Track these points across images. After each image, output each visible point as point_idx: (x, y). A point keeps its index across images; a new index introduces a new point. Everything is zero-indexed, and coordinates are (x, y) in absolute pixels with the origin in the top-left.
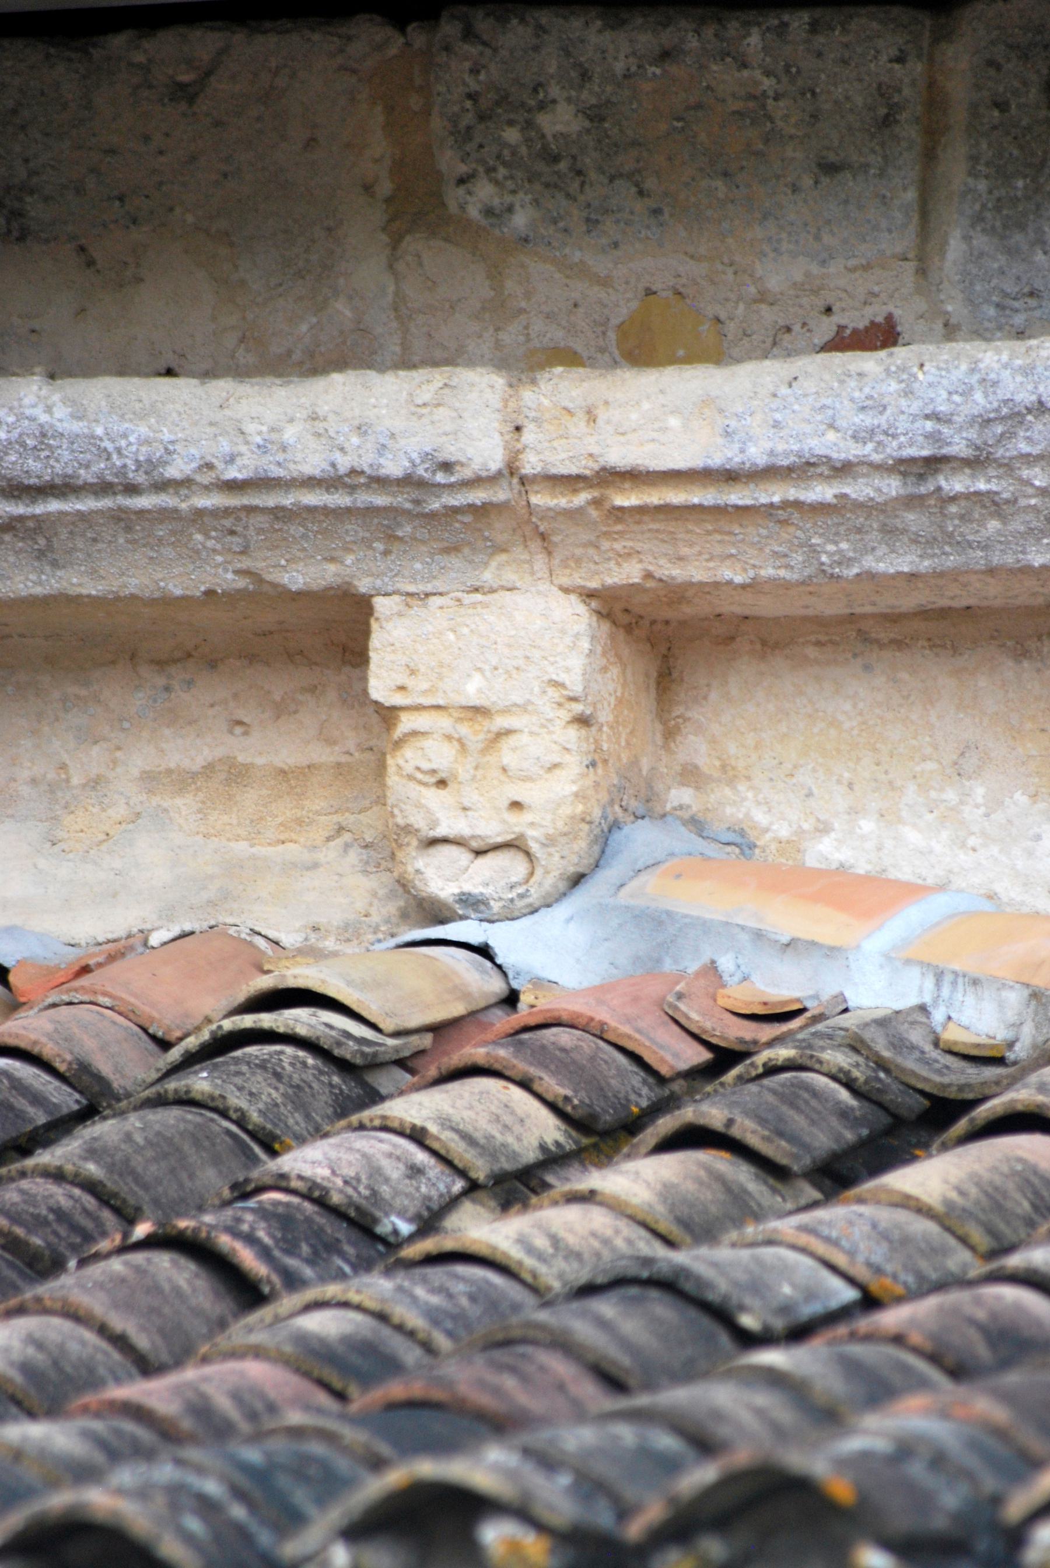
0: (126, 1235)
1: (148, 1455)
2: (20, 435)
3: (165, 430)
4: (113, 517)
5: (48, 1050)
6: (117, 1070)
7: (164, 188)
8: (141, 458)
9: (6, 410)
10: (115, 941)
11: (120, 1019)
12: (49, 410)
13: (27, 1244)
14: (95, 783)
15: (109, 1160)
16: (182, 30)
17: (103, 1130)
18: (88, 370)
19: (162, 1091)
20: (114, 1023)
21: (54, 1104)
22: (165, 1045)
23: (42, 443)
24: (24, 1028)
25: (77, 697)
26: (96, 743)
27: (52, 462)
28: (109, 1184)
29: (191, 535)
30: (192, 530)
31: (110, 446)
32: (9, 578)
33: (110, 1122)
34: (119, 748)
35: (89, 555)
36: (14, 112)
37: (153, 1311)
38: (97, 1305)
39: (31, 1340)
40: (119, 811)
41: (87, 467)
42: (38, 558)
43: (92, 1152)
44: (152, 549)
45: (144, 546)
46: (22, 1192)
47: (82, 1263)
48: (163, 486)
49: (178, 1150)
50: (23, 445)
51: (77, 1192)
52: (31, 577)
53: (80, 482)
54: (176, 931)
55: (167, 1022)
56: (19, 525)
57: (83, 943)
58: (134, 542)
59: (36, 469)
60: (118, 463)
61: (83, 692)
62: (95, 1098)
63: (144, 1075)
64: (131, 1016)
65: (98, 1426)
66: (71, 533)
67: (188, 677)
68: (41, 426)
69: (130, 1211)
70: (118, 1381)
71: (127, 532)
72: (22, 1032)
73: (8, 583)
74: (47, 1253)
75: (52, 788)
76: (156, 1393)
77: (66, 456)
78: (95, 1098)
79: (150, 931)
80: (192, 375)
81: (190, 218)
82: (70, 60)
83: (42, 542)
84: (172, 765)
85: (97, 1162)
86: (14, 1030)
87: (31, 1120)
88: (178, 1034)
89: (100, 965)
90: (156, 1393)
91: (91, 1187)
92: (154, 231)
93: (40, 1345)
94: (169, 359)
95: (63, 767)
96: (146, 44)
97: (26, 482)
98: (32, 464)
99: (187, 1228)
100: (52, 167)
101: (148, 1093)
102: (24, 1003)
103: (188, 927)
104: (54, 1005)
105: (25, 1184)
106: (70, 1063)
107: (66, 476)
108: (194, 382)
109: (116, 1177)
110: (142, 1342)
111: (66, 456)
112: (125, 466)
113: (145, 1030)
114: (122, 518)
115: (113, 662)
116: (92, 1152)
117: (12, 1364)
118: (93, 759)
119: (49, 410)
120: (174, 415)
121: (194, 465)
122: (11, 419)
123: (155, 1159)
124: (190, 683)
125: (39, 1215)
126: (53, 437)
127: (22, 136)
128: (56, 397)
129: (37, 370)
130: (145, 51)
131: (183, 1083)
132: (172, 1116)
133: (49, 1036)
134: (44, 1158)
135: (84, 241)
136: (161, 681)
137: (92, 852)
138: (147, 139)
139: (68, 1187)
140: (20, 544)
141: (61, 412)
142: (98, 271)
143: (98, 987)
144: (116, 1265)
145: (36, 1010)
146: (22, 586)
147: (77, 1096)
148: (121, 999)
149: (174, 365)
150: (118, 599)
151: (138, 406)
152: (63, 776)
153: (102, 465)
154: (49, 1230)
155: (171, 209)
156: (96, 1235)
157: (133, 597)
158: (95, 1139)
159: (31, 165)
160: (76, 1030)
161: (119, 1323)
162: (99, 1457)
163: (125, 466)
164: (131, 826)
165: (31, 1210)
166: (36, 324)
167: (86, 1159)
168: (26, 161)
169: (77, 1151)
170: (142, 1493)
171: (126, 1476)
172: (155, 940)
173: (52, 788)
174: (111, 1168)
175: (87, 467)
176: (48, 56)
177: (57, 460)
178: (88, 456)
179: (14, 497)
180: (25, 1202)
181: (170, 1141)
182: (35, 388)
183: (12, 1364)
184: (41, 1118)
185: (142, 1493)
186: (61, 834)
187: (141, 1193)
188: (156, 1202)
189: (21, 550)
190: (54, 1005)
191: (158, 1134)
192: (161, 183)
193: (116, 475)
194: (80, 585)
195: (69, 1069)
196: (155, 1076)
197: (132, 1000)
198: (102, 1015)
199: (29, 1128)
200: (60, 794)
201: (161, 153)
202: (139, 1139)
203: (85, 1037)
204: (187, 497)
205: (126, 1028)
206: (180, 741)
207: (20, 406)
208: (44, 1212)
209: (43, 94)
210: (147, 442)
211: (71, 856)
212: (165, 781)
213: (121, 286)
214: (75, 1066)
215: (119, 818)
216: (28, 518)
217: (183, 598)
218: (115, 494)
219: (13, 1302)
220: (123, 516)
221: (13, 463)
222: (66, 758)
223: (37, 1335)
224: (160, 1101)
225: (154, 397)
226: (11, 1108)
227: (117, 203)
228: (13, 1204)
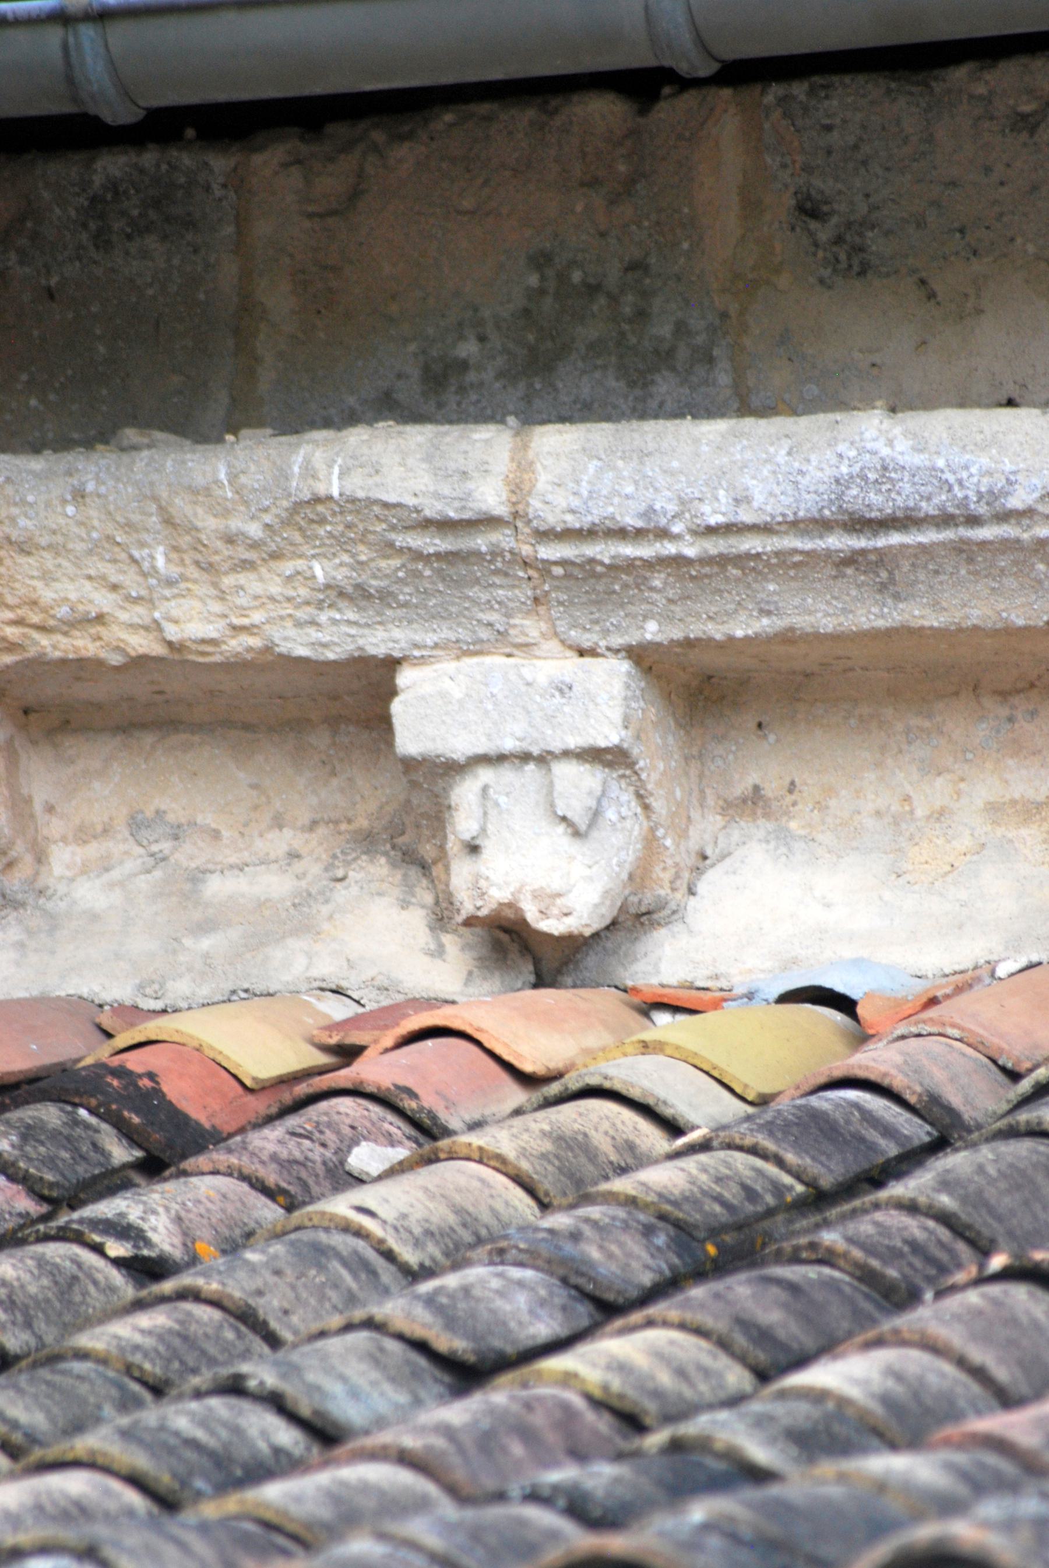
0: (982, 1266)
1: (1013, 1488)
2: (862, 469)
3: (1006, 460)
4: (954, 549)
5: (898, 1082)
6: (967, 1101)
7: (1005, 219)
8: (983, 489)
9: (847, 444)
10: (962, 972)
11: (970, 1051)
12: (890, 443)
13: (883, 1276)
14: (940, 814)
15: (962, 1192)
16: (1024, 60)
17: (955, 1161)
18: (928, 403)
19: (1013, 1122)
20: (964, 1055)
21: (906, 1136)
22: (1014, 1076)
23: (884, 476)
24: (874, 1060)
25: (921, 729)
26: (939, 774)
27: (893, 495)
28: (963, 1216)
29: (1033, 565)
30: (1034, 560)
31: (951, 478)
32: (851, 611)
33: (963, 1154)
34: (962, 780)
35: (931, 587)
36: (856, 147)
37: (1011, 1343)
38: (954, 1336)
39: (892, 1372)
40: (965, 842)
41: (929, 499)
42: (880, 591)
43: (945, 1184)
44: (994, 580)
45: (986, 577)
46: (877, 1224)
47: (939, 1295)
48: (1005, 516)
49: (1032, 1182)
50: (865, 478)
51: (931, 1224)
52: (873, 610)
53: (922, 515)
54: (1023, 962)
55: (1016, 1053)
56: (860, 559)
57: (930, 976)
58: (976, 573)
59: (876, 502)
60: (960, 495)
61: (927, 724)
62: (946, 1132)
63: (995, 1107)
64: (981, 1048)
65: (961, 1458)
66: (913, 565)
67: (1031, 708)
68: (883, 459)
69: (983, 1243)
70: (979, 1413)
71: (968, 563)
72: (872, 1064)
73: (851, 616)
74: (903, 1285)
75: (896, 822)
76: (1015, 1425)
77: (907, 488)
78: (946, 1132)
79: (997, 962)
80: (1033, 405)
81: (1031, 248)
82: (911, 94)
83: (884, 575)
84: (1017, 796)
85: (950, 1194)
86: (864, 1062)
87: (883, 1153)
88: (1027, 1065)
89: (947, 997)
90: (1015, 1425)
91: (945, 1218)
92: (995, 261)
93: (899, 1377)
94: (1010, 390)
95: (907, 799)
96: (987, 76)
97: (868, 516)
98: (874, 498)
99: (1043, 1261)
100: (893, 200)
101: (1001, 1124)
102: (873, 1036)
103: (1035, 958)
104: (903, 1037)
105: (879, 1216)
106: (920, 1095)
107: (907, 508)
108: (1036, 412)
109: (970, 1209)
110: (1001, 1374)
111: (907, 488)
112: (966, 497)
113: (994, 1062)
114: (963, 549)
115: (956, 694)
116: (945, 1184)
117: (873, 1396)
118: (936, 791)
119: (890, 443)
120: (1016, 445)
121: (1036, 495)
122: (853, 453)
123: (1009, 1191)
124: (1033, 714)
125: (894, 1247)
126: (895, 470)
127: (862, 171)
128: (897, 430)
129: (879, 403)
130: (987, 83)
131: (1035, 1114)
132: (1023, 1148)
133: (898, 1067)
134: (897, 1189)
135: (924, 274)
136: (1004, 712)
137: (937, 884)
138: (988, 170)
139: (922, 1219)
140: (862, 578)
141: (902, 445)
142: (938, 303)
143: (947, 1019)
144: (973, 1297)
145: (885, 1042)
146: (864, 619)
147: (928, 1128)
148: (970, 1031)
149: (1015, 395)
150: (960, 630)
151: (979, 437)
152: (907, 808)
153: (944, 497)
154: (904, 1263)
155: (1012, 240)
156: (951, 1267)
157: (976, 628)
158: (947, 1171)
159: (871, 200)
160: (925, 1062)
161: (978, 1355)
162: (962, 1490)
163: (966, 497)
164: (975, 858)
165: (887, 1242)
166: (877, 358)
167: (939, 1191)
168: (867, 196)
169: (931, 1183)
170: (1009, 1525)
171: (991, 1508)
172: (1002, 971)
173: (896, 822)
174: (964, 1200)
175: (929, 499)
176: (889, 91)
177: (899, 493)
178: (930, 488)
179: (855, 530)
180: (880, 1234)
181: (1022, 1173)
182: (876, 421)
183: (873, 1396)
184: (892, 1150)
185: (1009, 1525)
186: (906, 866)
187: (995, 1225)
188: (1011, 1234)
189: (863, 582)
190: (903, 1037)
191: (1011, 1166)
192: (1001, 215)
193: (958, 507)
194: (922, 617)
195: (920, 1101)
196: (1005, 1107)
197: (981, 1031)
198: (951, 1046)
199: (881, 1160)
200: (904, 826)
201: (1002, 184)
202: (992, 1170)
203: (935, 1069)
204: (1029, 526)
205: (976, 1060)
206: (1024, 772)
207: (862, 440)
208: (899, 1244)
209: (884, 129)
210: (989, 473)
211: (916, 887)
212: (1010, 811)
213: (961, 318)
214: (925, 1098)
215: (964, 849)
216: (870, 551)
217: (1026, 628)
218: (956, 525)
219: (871, 1334)
220: (965, 547)
221: (855, 497)
222: (909, 789)
223: (897, 1367)
224: (1012, 1133)
225: (996, 428)
226: (862, 1140)
227: (958, 235)
228: (867, 1236)
